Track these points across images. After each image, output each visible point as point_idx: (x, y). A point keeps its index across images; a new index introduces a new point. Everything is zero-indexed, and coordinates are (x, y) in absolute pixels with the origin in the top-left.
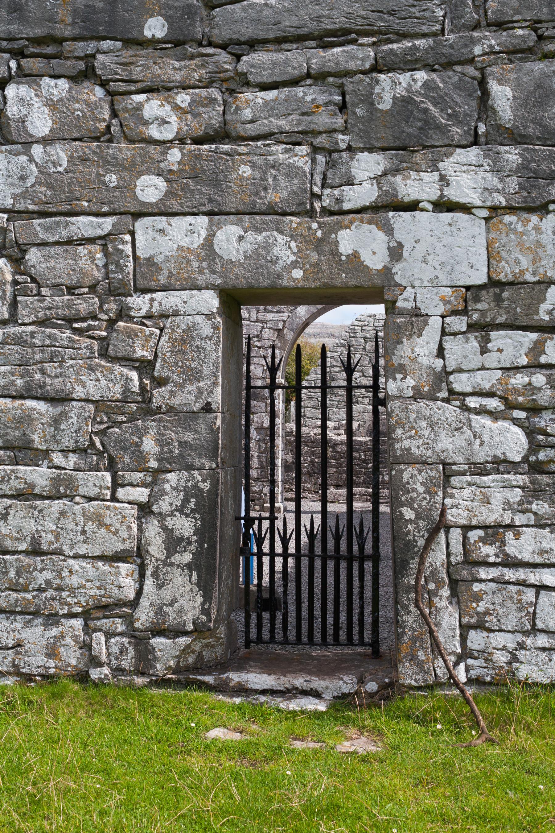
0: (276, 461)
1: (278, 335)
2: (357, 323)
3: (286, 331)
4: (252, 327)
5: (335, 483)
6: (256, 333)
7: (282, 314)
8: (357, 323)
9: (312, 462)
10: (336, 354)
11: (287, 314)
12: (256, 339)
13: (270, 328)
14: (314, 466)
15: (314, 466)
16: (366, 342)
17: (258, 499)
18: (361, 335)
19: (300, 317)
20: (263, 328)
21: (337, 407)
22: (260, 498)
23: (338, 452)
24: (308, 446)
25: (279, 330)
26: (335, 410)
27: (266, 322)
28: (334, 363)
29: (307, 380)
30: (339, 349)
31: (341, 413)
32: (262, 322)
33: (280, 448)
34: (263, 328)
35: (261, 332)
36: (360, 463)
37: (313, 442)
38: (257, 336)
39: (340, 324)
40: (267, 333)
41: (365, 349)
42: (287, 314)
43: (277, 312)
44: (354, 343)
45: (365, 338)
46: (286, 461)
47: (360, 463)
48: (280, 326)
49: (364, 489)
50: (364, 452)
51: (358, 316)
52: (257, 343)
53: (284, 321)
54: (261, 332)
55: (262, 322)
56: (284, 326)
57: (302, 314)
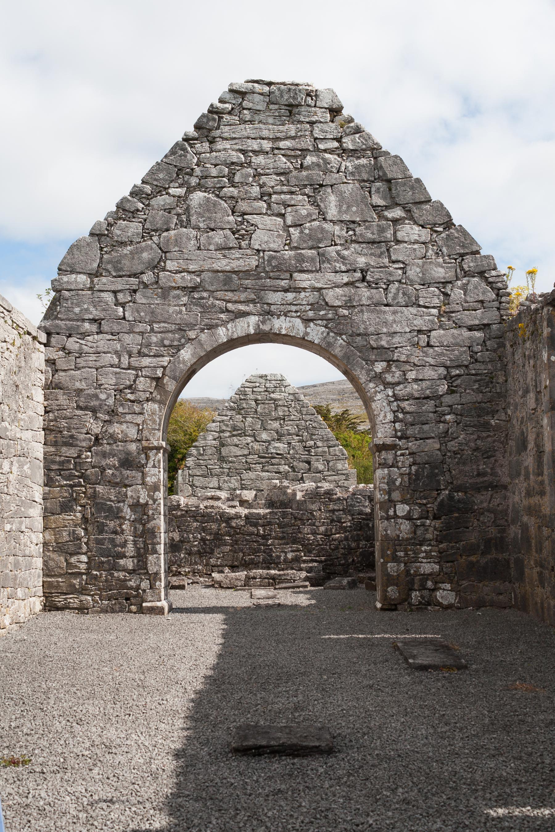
0: (158, 547)
1: (157, 385)
2: (248, 384)
3: (166, 379)
4: (123, 376)
5: (230, 563)
6: (128, 383)
7: (160, 359)
8: (248, 384)
9: (203, 540)
10: (225, 418)
11: (167, 359)
12: (128, 391)
13: (146, 377)
14: (205, 544)
15: (205, 544)
16: (257, 404)
17: (135, 597)
18: (252, 397)
19: (184, 362)
20: (137, 376)
21: (228, 475)
22: (138, 596)
23: (232, 527)
24: (197, 521)
25: (158, 379)
26: (226, 478)
27: (141, 369)
28: (224, 428)
29: (195, 447)
30: (229, 413)
31: (233, 481)
32: (135, 369)
33: (162, 530)
34: (137, 376)
35: (135, 381)
36: (259, 539)
37: (203, 516)
38: (130, 387)
39: (341, 100)
40: (142, 383)
41: (256, 411)
42: (167, 359)
43: (154, 356)
44: (244, 405)
45: (256, 400)
46: (173, 539)
47: (259, 539)
48: (159, 373)
49: (265, 571)
50: (262, 526)
51: (248, 377)
52: (129, 396)
53: (164, 368)
54: (135, 381)
55: (135, 369)
56: (163, 374)
57: (186, 358)
